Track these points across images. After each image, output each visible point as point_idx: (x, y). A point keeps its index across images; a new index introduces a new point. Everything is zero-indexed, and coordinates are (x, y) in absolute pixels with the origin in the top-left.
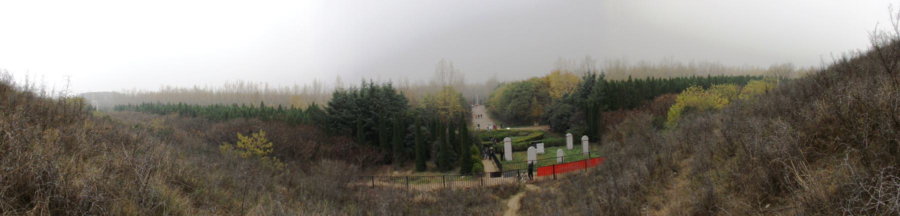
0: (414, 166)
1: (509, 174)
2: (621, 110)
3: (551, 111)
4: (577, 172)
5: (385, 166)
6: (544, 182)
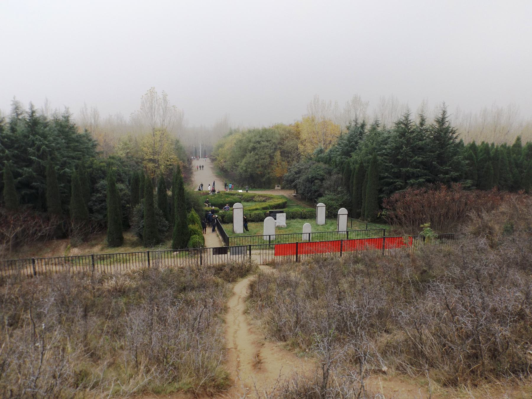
0: (105, 241)
1: (238, 250)
2: (495, 189)
3: (299, 172)
4: (327, 255)
5: (55, 242)
6: (282, 264)
